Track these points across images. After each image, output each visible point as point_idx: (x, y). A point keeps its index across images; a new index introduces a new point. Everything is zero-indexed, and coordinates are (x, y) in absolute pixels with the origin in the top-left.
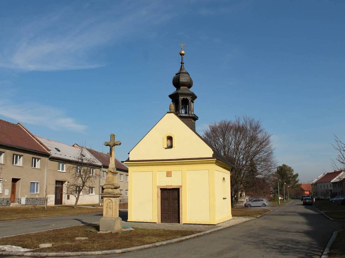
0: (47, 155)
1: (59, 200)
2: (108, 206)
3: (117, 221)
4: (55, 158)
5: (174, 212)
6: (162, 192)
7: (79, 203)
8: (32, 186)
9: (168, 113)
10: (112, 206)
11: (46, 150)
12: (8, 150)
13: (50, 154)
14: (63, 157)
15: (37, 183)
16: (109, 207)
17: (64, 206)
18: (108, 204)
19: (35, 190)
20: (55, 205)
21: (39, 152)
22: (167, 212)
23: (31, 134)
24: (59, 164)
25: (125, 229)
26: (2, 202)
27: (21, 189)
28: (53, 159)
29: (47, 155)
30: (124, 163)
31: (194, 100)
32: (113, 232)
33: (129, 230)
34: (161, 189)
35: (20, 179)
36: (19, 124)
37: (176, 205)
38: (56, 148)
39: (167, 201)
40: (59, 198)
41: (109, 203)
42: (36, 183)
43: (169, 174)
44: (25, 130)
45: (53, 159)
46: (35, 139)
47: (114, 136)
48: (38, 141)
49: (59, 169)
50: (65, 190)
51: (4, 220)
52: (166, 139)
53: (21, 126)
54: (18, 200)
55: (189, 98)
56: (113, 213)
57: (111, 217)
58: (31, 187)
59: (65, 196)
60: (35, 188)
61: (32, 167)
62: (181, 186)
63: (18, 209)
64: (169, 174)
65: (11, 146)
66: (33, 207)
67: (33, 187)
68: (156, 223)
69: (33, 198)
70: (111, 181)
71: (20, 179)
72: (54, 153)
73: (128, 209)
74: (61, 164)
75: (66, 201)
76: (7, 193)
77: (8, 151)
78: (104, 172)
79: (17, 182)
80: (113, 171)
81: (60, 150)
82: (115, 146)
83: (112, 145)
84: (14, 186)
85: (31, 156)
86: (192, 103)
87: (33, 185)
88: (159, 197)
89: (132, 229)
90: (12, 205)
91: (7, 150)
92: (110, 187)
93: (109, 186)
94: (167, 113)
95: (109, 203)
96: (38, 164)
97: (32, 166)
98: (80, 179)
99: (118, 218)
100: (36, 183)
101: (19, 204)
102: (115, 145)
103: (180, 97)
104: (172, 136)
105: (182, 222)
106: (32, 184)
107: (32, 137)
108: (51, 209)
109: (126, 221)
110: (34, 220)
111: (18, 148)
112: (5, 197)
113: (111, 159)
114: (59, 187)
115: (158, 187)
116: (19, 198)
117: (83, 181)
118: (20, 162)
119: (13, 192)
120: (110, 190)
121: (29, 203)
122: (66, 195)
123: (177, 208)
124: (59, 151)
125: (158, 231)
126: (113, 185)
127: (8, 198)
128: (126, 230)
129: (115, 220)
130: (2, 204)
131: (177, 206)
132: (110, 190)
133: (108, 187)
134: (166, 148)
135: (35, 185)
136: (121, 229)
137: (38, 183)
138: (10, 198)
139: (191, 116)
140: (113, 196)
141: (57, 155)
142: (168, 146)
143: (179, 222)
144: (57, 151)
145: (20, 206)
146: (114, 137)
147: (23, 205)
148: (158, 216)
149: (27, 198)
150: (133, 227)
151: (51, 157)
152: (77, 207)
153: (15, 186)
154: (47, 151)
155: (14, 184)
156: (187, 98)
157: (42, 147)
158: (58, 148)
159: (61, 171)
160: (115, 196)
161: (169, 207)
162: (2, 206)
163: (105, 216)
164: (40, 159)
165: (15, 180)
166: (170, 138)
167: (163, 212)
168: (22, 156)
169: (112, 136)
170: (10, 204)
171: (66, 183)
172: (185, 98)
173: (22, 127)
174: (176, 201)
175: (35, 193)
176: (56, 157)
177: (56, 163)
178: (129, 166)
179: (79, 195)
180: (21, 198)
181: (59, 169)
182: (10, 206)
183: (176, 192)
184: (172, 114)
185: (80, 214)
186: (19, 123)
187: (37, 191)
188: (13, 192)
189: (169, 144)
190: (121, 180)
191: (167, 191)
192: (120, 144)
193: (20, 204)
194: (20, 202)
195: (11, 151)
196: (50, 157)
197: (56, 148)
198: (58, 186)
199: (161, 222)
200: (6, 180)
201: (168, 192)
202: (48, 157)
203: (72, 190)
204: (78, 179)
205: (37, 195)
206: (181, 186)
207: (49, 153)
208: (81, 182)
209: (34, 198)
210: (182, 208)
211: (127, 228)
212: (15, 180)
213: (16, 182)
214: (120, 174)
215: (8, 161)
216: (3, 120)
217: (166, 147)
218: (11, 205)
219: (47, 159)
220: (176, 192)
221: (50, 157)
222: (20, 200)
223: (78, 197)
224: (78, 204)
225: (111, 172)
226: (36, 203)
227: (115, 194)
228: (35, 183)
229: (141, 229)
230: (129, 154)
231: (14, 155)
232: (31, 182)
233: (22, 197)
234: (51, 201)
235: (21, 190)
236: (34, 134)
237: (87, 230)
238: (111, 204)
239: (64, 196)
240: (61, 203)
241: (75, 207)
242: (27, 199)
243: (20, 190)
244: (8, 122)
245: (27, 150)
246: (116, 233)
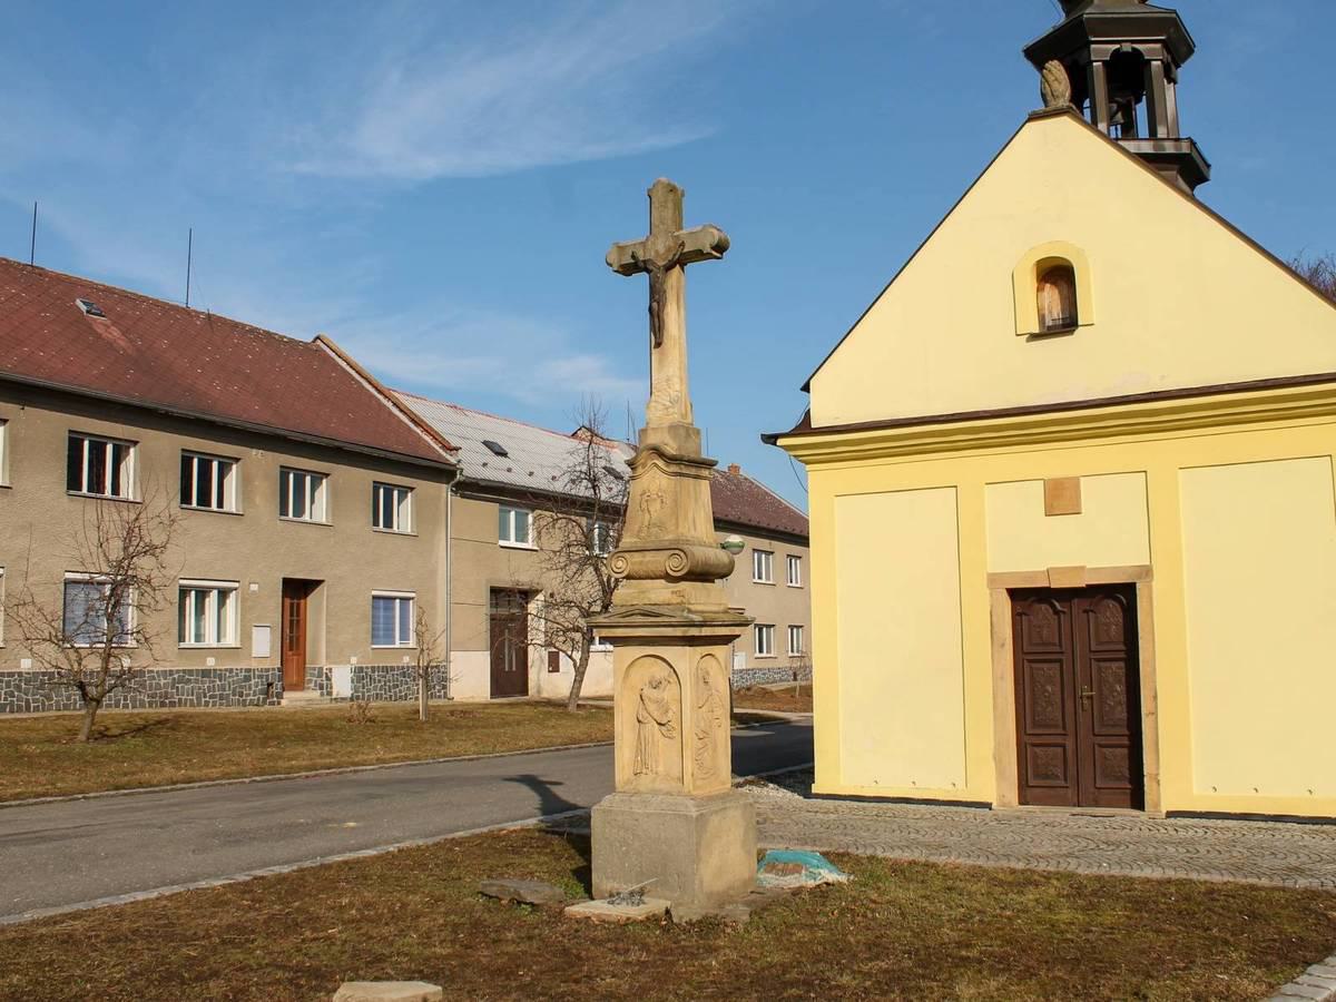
0: (441, 472)
1: (509, 678)
2: (652, 707)
3: (714, 821)
4: (483, 484)
5: (1103, 741)
6: (1020, 614)
7: (586, 690)
8: (382, 613)
9: (1034, 117)
10: (674, 707)
11: (437, 448)
12: (254, 451)
13: (455, 465)
14: (519, 479)
15: (401, 599)
16: (656, 715)
17: (537, 704)
18: (648, 692)
19: (393, 630)
20: (493, 695)
21: (403, 459)
22: (1059, 740)
23: (370, 383)
24: (501, 511)
25: (785, 872)
26: (241, 687)
27: (328, 627)
28: (473, 489)
29: (441, 472)
30: (780, 442)
31: (1178, 66)
32: (682, 915)
33: (811, 883)
34: (1014, 594)
35: (323, 581)
36: (319, 342)
37: (1113, 690)
38: (486, 443)
39: (1057, 665)
40: (510, 664)
41: (656, 685)
42: (398, 601)
43: (1061, 498)
44: (344, 364)
45: (473, 489)
46: (389, 405)
47: (671, 196)
48: (401, 411)
49: (505, 537)
50: (537, 630)
51: (141, 785)
52: (1029, 280)
53: (328, 350)
54: (320, 676)
55: (1152, 50)
56: (689, 766)
57: (669, 793)
58: (375, 618)
59: (537, 656)
60: (394, 623)
61: (375, 528)
62: (1147, 571)
63: (283, 721)
64: (1061, 498)
65: (266, 430)
66: (355, 712)
67: (386, 617)
68: (988, 806)
69: (386, 669)
70: (661, 526)
71: (323, 581)
72: (474, 463)
73: (815, 714)
74: (513, 514)
75: (546, 682)
76: (264, 646)
77: (255, 455)
78: (795, 630)
79: (309, 599)
80: (679, 448)
81: (507, 450)
82: (689, 267)
83: (661, 263)
84: (298, 615)
85: (365, 477)
86: (1169, 83)
87: (386, 609)
88: (1003, 645)
89: (830, 875)
90: (291, 700)
91: (252, 448)
92: (659, 569)
93: (649, 557)
94: (1029, 120)
95: (656, 685)
96: (405, 516)
97: (376, 523)
98: (589, 571)
99: (723, 797)
100: (398, 601)
101: (322, 694)
102: (682, 260)
103: (1093, 46)
104: (1072, 261)
105: (1157, 805)
106: (382, 602)
107: (376, 393)
108: (466, 717)
109: (808, 794)
110: (327, 779)
111: (300, 438)
112: (254, 665)
113: (661, 362)
114: (512, 618)
115: (993, 579)
116: (321, 669)
117: (602, 583)
118: (319, 507)
119: (293, 638)
120: (659, 592)
121: (369, 691)
122: (545, 654)
123: (1121, 713)
124: (504, 454)
125: (1030, 895)
126: (676, 548)
127: (267, 670)
128: (791, 881)
129: (701, 820)
130: (241, 695)
131: (1123, 698)
132: (659, 592)
133: (641, 570)
134: (1034, 337)
135: (393, 609)
136: (752, 879)
137: (409, 599)
138: (279, 670)
139: (1169, 148)
140: (679, 632)
141: (495, 472)
142: (1049, 322)
143: (1138, 801)
144: (490, 452)
145: (326, 704)
146: (678, 207)
147: (343, 699)
148: (998, 759)
149: (361, 669)
150: (841, 842)
151: (462, 479)
152: (578, 705)
153: (302, 617)
154: (444, 454)
155: (298, 605)
156: (1136, 46)
157: (420, 437)
158: (500, 444)
159: (512, 543)
160: (694, 632)
161: (1069, 705)
162: (245, 705)
163: (629, 782)
164: (412, 489)
165: (296, 589)
166: (1057, 274)
167: (1026, 739)
168: (327, 475)
169: (659, 195)
170: (279, 696)
171: (540, 597)
172: (1127, 48)
173: (333, 355)
174: (1114, 665)
175: (397, 645)
176: (485, 480)
177: (488, 510)
178: (807, 463)
179: (586, 653)
180: (331, 669)
181: (505, 537)
182: (279, 703)
183: (1112, 612)
184: (1065, 120)
185: (580, 741)
186: (318, 338)
187: (404, 636)
188: (293, 638)
189: (1055, 312)
190: (794, 584)
191: (1053, 606)
192: (721, 248)
193: (330, 693)
194: (325, 687)
195: (270, 455)
196: (456, 480)
197: (486, 443)
198: (503, 611)
199: (1021, 803)
200: (254, 587)
201: (1056, 612)
202: (448, 483)
203: (556, 625)
204: (580, 571)
205: (404, 655)
206: (1147, 571)
207: (453, 460)
208: (596, 591)
209: (392, 669)
210: (1154, 713)
211: (797, 869)
212: (296, 589)
213: (306, 595)
214: (788, 555)
215: (258, 500)
216: (244, 326)
217: (1036, 330)
218: (284, 702)
219: (443, 490)
220: (1112, 612)
221: (456, 480)
222: (328, 679)
223: (585, 660)
224: (582, 694)
225: (658, 452)
226: (400, 692)
227: (697, 618)
228: (395, 598)
229: (897, 869)
230: (806, 388)
231: (285, 471)
232: (374, 597)
233: (335, 663)
234: (470, 678)
235: (328, 632)
236: (384, 384)
237: (493, 891)
238: (668, 693)
239: (533, 653)
240: (525, 691)
241: (572, 708)
242: (360, 675)
243: (324, 633)
244: (268, 332)
245: (349, 447)
246: (706, 917)
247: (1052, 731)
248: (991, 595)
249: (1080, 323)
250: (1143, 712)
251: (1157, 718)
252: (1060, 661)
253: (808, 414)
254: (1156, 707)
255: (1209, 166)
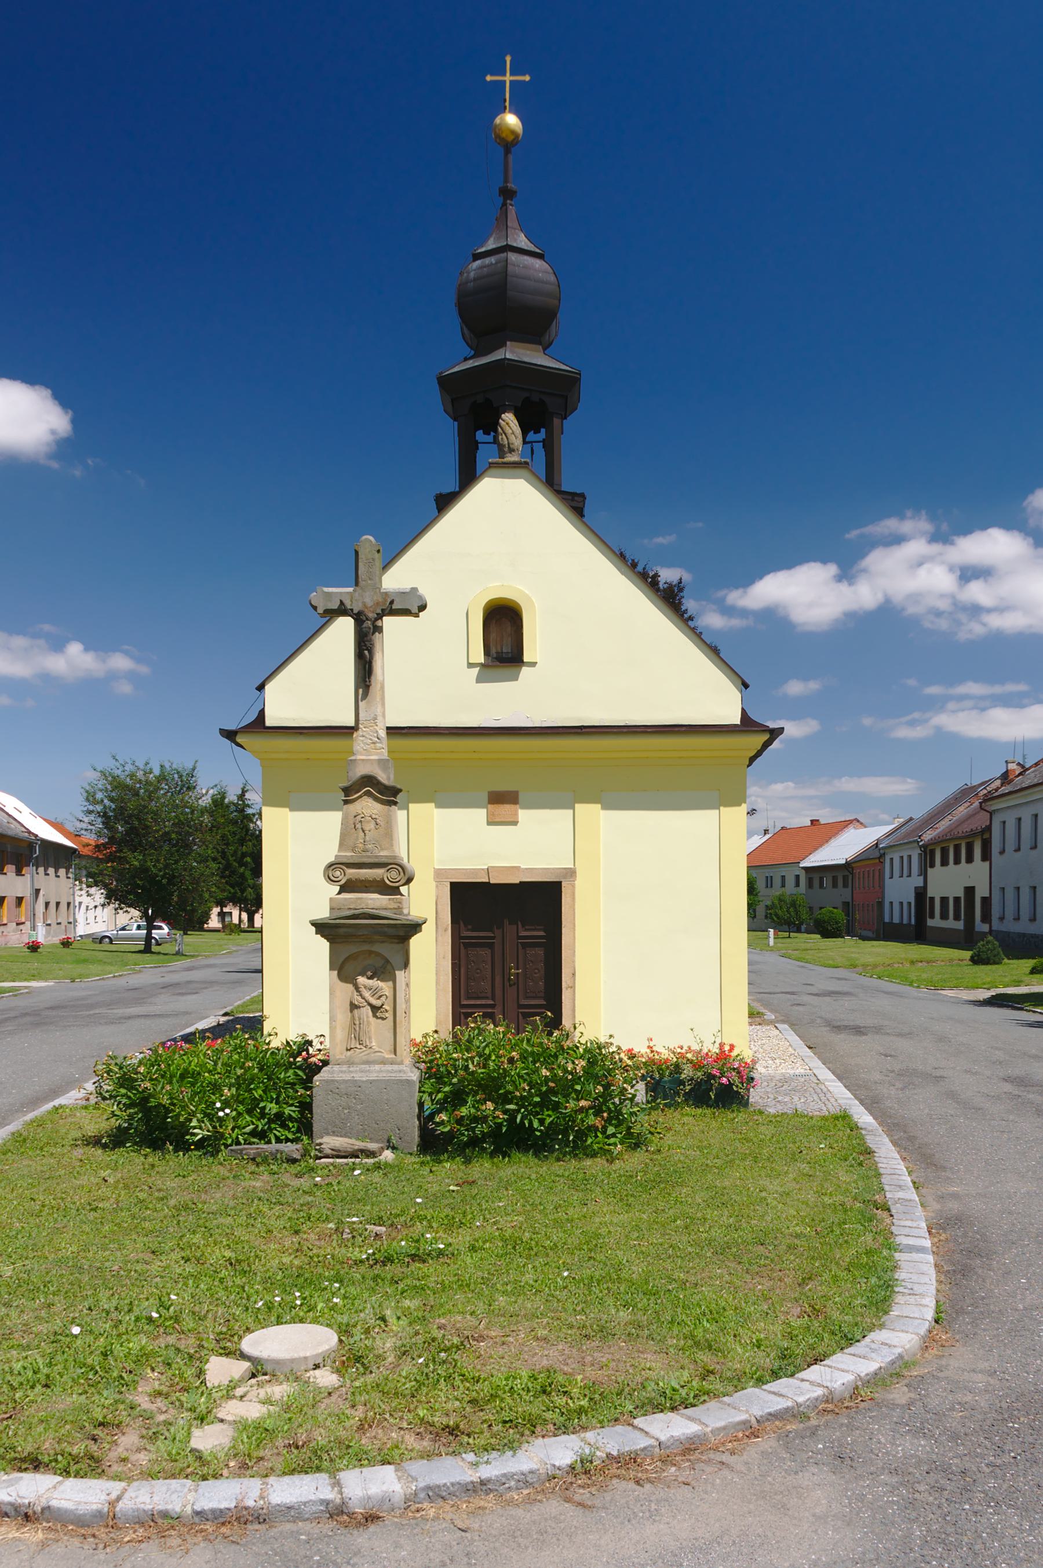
62: (571, 873)
115: (439, 874)
206: (571, 873)
210: (573, 987)
230: (261, 688)
247: (483, 1002)
248: (437, 886)
249: (526, 658)
250: (564, 984)
251: (574, 991)
252: (491, 946)
253: (262, 713)
254: (574, 983)
255: (911, 819)
